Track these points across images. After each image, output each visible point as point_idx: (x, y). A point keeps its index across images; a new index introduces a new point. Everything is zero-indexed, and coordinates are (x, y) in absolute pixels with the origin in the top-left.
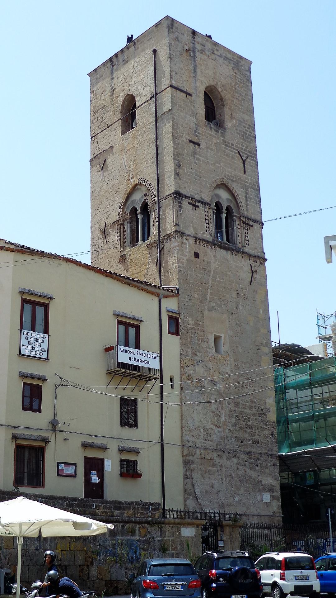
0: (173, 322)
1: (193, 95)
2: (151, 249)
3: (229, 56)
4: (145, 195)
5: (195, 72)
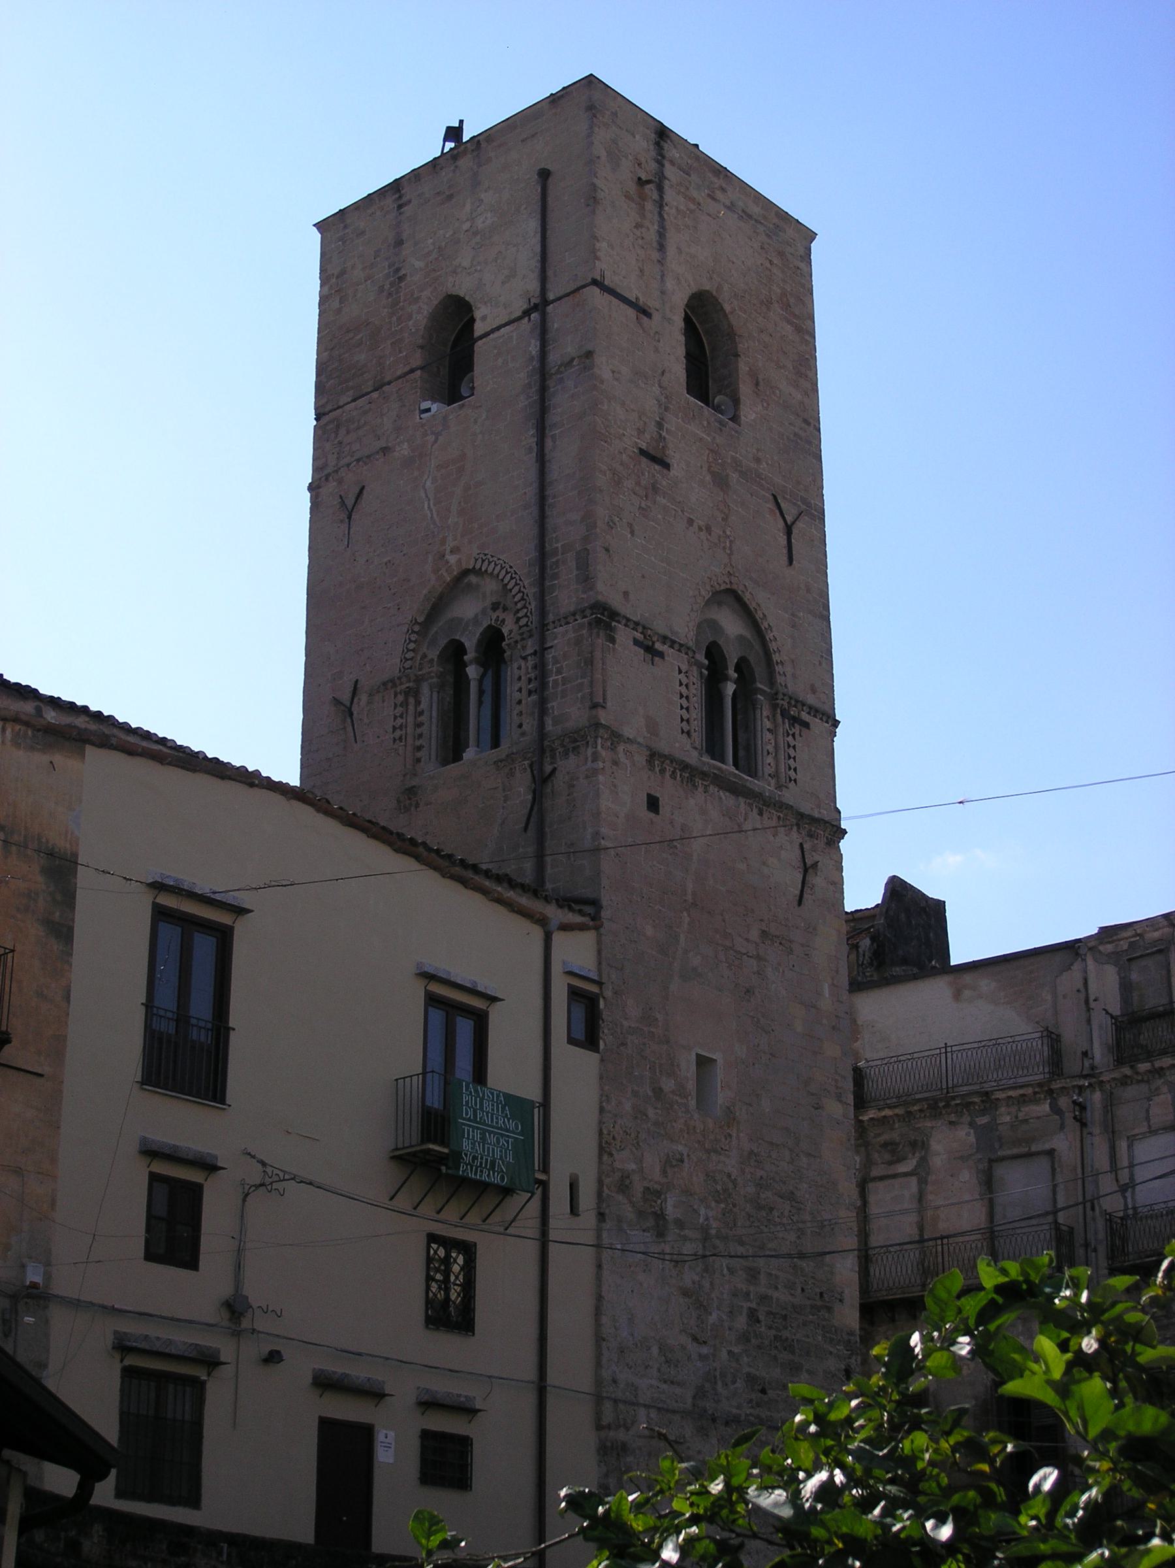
0: (580, 1012)
1: (656, 316)
2: (511, 774)
3: (756, 210)
4: (495, 607)
5: (661, 247)
